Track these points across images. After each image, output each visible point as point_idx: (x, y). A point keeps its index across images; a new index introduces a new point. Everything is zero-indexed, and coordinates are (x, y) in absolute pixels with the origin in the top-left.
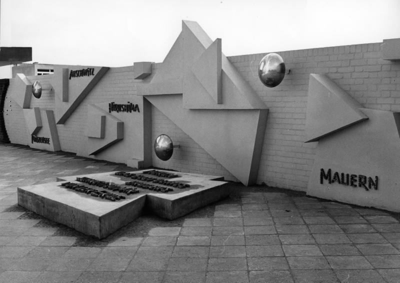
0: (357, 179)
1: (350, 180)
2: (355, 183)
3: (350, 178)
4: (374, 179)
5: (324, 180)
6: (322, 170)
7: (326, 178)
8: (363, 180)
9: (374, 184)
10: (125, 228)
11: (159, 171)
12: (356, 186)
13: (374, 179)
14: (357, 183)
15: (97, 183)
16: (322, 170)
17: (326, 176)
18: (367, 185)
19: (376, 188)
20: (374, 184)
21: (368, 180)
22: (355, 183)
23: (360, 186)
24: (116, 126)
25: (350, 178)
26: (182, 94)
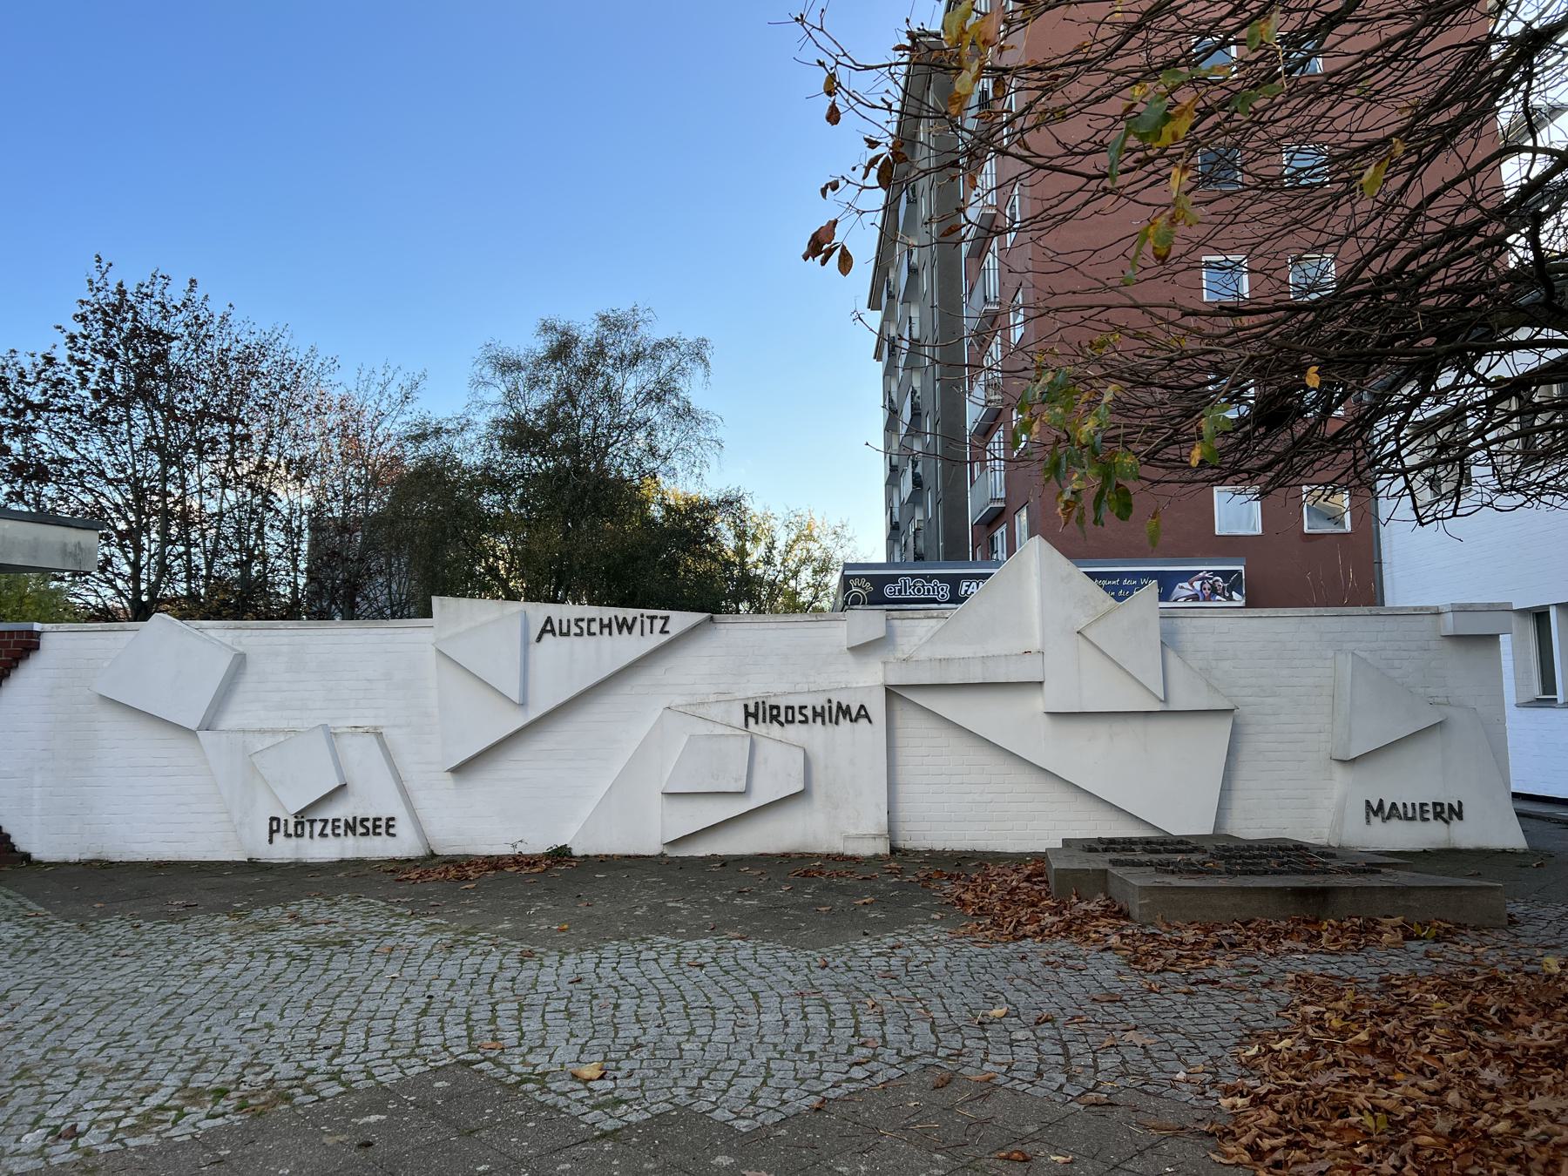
0: (1430, 808)
1: (1418, 813)
2: (1426, 816)
3: (1417, 808)
4: (1456, 807)
5: (1373, 819)
6: (1368, 802)
7: (1376, 814)
8: (1439, 809)
9: (1457, 812)
10: (917, 320)
11: (1222, 882)
12: (380, 834)
13: (351, 821)
14: (1430, 816)
15: (896, 412)
16: (1368, 802)
17: (1375, 811)
18: (1445, 815)
19: (1460, 817)
20: (1457, 812)
21: (1446, 807)
22: (337, 831)
23: (1435, 818)
24: (434, 610)
25: (1417, 808)
26: (1041, 683)
